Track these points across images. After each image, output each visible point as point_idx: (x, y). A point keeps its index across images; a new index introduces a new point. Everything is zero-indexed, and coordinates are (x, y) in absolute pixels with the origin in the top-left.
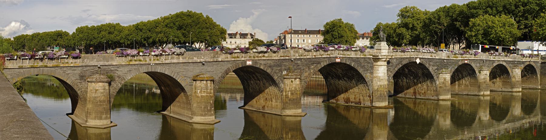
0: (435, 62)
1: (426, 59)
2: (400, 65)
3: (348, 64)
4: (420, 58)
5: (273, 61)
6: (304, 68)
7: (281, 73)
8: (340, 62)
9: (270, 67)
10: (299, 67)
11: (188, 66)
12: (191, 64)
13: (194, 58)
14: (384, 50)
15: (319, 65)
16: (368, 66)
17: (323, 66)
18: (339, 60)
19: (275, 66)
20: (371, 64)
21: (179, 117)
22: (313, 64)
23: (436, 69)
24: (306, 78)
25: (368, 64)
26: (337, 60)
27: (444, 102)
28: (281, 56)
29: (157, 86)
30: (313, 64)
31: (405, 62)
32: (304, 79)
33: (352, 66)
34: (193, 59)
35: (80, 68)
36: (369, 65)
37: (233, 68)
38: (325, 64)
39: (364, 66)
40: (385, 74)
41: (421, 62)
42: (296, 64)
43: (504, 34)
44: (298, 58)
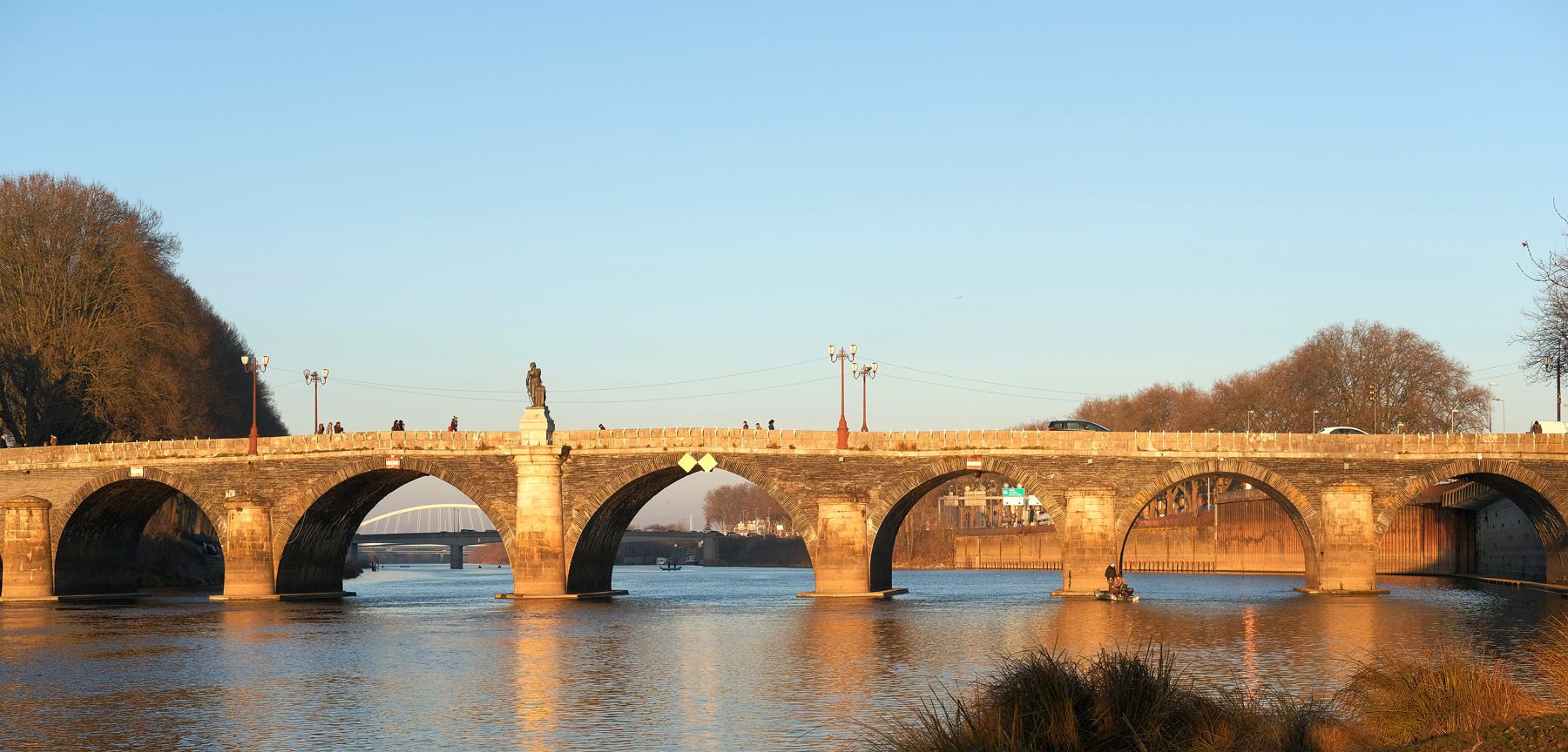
0: (792, 466)
6: (287, 483)
7: (220, 496)
8: (397, 468)
9: (192, 480)
10: (272, 482)
13: (10, 462)
14: (531, 433)
15: (331, 476)
16: (498, 478)
17: (343, 478)
20: (509, 473)
21: (715, 573)
22: (311, 473)
24: (293, 511)
26: (388, 463)
27: (431, 608)
28: (219, 456)
30: (311, 473)
32: (285, 512)
34: (7, 463)
36: (501, 476)
37: (97, 484)
39: (481, 478)
40: (1368, 511)
42: (262, 473)
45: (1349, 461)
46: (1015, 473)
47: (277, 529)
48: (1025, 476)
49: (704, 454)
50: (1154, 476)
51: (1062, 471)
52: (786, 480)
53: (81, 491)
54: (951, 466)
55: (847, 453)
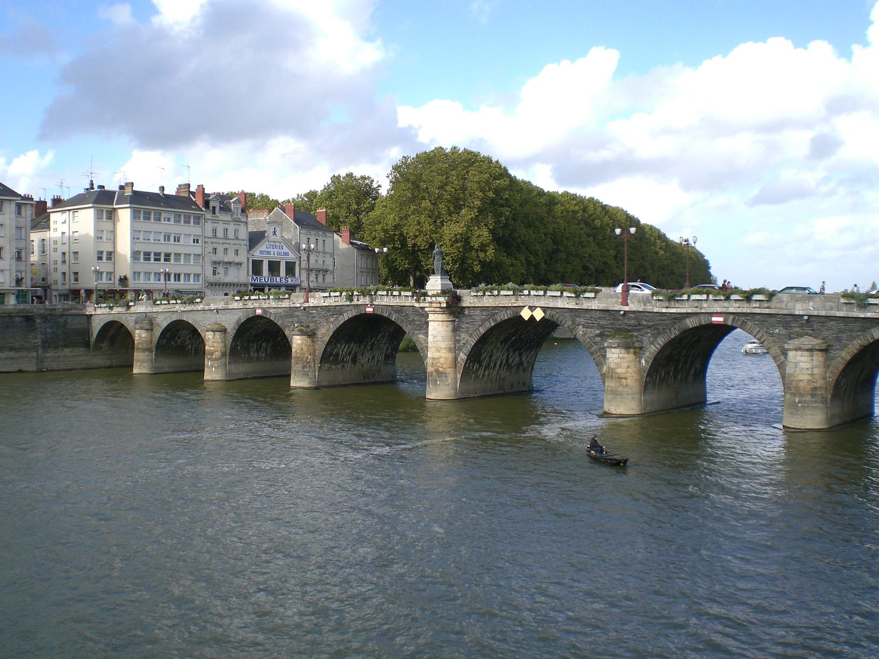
1: (593, 314)
2: (492, 322)
3: (387, 316)
4: (544, 309)
5: (284, 309)
11: (206, 314)
12: (208, 312)
17: (347, 319)
18: (371, 310)
19: (286, 316)
23: (597, 336)
25: (421, 317)
29: (93, 236)
31: (502, 317)
33: (393, 320)
35: (135, 315)
38: (350, 316)
39: (413, 320)
41: (547, 317)
43: (557, 272)
44: (655, 311)
45: (488, 642)
46: (749, 327)
47: (317, 347)
48: (757, 330)
49: (536, 307)
50: (859, 333)
51: (785, 328)
52: (588, 328)
53: (238, 321)
54: (700, 321)
55: (626, 308)
